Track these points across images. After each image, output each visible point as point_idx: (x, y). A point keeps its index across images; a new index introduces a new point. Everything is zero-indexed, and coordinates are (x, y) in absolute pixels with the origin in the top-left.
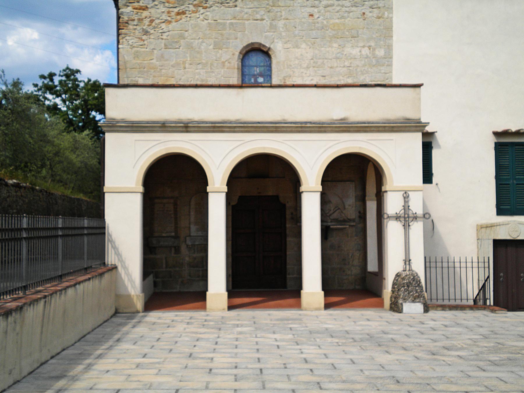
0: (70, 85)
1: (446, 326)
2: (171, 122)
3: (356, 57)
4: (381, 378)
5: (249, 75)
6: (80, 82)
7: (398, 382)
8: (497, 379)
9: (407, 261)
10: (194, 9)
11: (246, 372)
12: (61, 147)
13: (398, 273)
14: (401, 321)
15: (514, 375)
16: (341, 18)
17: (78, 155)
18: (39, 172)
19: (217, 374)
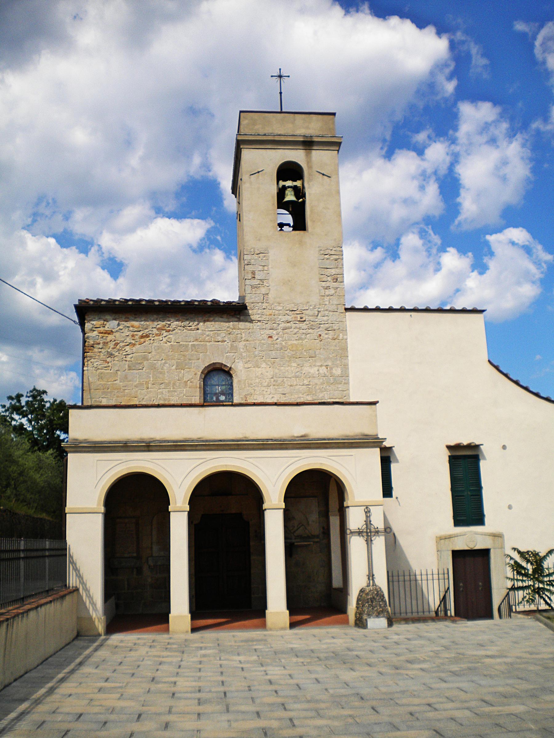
0: (36, 406)
1: (409, 639)
2: (133, 441)
3: (314, 376)
4: (345, 696)
5: (211, 394)
6: (47, 402)
7: (362, 698)
8: (458, 690)
9: (371, 576)
10: (157, 332)
11: (209, 696)
12: (25, 467)
13: (362, 589)
14: (366, 637)
15: (473, 684)
16: (298, 340)
17: (42, 475)
18: (4, 492)
19: (180, 698)
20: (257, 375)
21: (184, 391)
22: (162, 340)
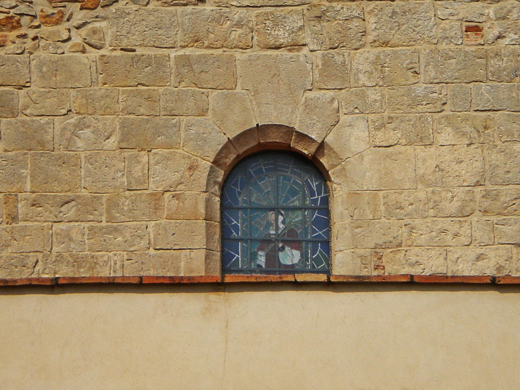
10: (50, 10)
20: (421, 172)
21: (150, 230)
22: (69, 39)
